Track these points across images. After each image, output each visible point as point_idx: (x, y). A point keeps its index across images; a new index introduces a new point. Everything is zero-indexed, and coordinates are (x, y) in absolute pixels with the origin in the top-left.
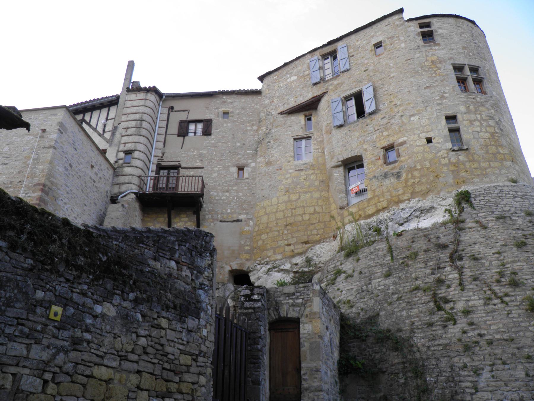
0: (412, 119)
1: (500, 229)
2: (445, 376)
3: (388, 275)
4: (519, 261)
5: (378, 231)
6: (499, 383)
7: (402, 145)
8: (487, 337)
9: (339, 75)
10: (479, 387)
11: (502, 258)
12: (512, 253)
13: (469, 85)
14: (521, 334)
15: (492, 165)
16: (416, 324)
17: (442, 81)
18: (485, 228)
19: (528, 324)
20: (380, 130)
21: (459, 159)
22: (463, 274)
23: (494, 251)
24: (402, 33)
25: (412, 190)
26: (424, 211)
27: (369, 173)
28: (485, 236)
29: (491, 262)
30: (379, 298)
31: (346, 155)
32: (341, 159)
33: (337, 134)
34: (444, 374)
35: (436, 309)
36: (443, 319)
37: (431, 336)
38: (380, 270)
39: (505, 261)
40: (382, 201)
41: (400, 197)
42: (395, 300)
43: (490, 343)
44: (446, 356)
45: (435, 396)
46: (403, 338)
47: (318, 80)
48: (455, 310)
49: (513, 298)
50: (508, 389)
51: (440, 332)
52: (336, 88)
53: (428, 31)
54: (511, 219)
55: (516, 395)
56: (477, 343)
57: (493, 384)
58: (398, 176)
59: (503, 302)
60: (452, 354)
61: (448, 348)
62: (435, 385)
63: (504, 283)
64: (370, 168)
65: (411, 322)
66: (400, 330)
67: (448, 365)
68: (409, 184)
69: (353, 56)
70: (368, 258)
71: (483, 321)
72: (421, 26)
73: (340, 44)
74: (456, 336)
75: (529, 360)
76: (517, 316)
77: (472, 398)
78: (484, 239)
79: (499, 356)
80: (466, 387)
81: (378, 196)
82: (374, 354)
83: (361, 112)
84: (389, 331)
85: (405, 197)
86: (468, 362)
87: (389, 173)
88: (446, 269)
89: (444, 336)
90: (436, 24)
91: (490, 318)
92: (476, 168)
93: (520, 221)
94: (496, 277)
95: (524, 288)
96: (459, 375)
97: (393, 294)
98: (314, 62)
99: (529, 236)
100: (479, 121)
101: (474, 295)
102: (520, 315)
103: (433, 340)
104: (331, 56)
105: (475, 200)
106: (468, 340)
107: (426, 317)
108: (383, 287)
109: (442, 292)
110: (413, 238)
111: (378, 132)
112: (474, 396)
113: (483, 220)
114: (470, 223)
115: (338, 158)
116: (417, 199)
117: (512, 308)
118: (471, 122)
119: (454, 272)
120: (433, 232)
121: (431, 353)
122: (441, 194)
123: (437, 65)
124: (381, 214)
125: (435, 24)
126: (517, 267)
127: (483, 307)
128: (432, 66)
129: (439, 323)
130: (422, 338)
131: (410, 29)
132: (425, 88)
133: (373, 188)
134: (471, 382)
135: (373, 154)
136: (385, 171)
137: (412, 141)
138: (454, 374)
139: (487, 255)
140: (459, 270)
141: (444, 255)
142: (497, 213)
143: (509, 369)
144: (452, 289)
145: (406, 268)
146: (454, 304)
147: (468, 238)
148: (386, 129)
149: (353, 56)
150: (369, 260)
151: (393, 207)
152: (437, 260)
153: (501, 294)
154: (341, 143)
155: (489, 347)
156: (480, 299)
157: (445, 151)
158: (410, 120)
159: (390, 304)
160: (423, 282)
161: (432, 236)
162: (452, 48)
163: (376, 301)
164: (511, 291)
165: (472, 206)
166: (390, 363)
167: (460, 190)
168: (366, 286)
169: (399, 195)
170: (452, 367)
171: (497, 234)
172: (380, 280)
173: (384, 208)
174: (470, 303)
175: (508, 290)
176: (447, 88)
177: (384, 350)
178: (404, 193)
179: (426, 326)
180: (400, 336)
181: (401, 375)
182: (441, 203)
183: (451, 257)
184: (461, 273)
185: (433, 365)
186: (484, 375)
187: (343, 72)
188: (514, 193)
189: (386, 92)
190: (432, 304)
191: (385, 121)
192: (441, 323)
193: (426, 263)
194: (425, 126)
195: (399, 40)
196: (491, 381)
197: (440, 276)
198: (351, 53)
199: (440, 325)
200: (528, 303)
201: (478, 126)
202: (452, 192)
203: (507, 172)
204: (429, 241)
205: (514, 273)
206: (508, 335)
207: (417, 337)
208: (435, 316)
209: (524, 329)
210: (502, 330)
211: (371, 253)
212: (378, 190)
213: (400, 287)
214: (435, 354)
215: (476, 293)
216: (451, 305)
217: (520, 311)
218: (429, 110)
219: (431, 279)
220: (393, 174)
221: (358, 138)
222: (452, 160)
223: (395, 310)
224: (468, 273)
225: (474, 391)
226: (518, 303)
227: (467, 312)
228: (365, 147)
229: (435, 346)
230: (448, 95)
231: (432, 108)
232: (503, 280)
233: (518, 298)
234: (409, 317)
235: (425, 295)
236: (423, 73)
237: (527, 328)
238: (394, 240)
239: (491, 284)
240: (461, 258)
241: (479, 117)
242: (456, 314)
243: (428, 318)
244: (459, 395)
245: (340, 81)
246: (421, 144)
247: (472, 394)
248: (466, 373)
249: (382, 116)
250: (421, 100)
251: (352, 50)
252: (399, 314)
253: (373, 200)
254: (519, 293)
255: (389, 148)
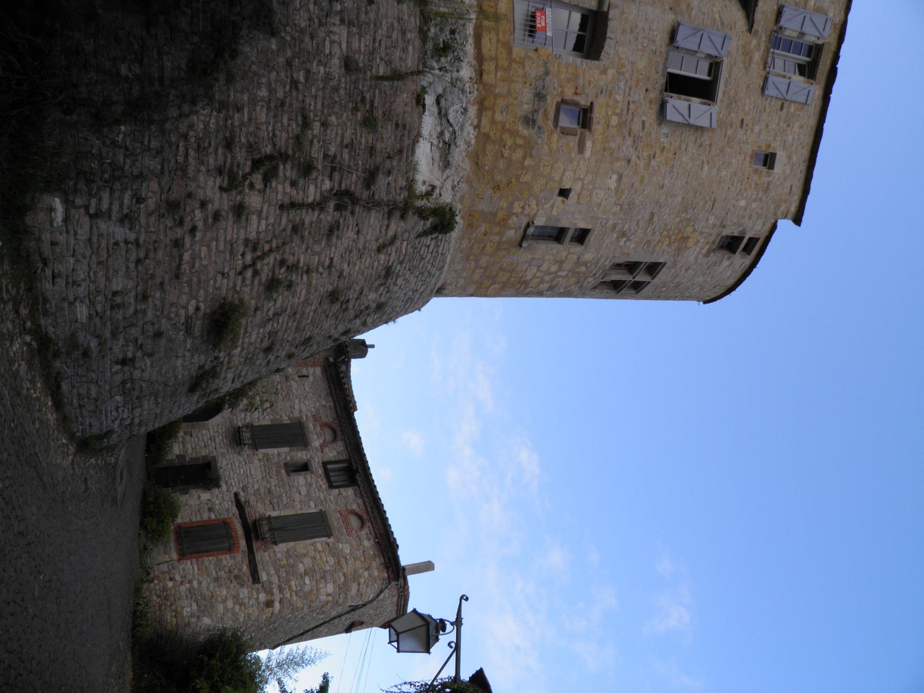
0: (615, 177)
1: (370, 271)
2: (125, 163)
3: (349, 64)
4: (308, 292)
5: (444, 50)
6: (104, 255)
7: (579, 145)
8: (188, 240)
9: (765, 68)
10: (99, 221)
11: (321, 270)
12: (323, 283)
13: (618, 274)
14: (187, 290)
15: (479, 271)
16: (236, 116)
17: (648, 242)
18: (379, 250)
19: (200, 299)
20: (625, 112)
21: (510, 228)
22: (310, 210)
23: (335, 260)
24: (762, 208)
25: (493, 138)
26: (446, 148)
27: (559, 65)
28: (365, 248)
29: (319, 254)
30: (307, 39)
31: (614, 27)
32: (611, 14)
33: (662, 21)
34: (128, 161)
35: (258, 157)
36: (235, 169)
37: (206, 144)
38: (362, 49)
39: (314, 274)
40: (496, 75)
41: (489, 113)
42: (295, 75)
43: (177, 243)
44: (162, 168)
45: (86, 139)
46: (212, 87)
47: (783, 22)
48: (247, 190)
49: (248, 282)
50: (94, 267)
51: (211, 161)
52: (747, 54)
53: (738, 247)
54: (381, 285)
55: (82, 276)
56: (181, 223)
57: (104, 244)
58: (529, 121)
59: (245, 267)
60: (165, 180)
61: (179, 173)
62: (108, 142)
63: (277, 271)
64: (567, 68)
65: (243, 105)
66: (230, 79)
67: (145, 171)
68: (506, 136)
69: (782, 108)
70: (396, 25)
71: (217, 236)
72: (752, 241)
73: (817, 90)
74: (199, 190)
75: (140, 297)
76: (217, 286)
77: (80, 207)
78: (361, 247)
79: (152, 255)
80: (100, 199)
81: (508, 69)
82: (189, 12)
83: (679, 85)
84: (234, 54)
85: (485, 122)
86: (146, 206)
87: (542, 104)
88: (327, 182)
89: (203, 168)
90: (740, 261)
91: (222, 248)
92: (484, 248)
93: (372, 296)
94: (291, 260)
95: (262, 297)
96: (124, 189)
97: (308, 71)
98: (821, 27)
99: (344, 306)
100: (556, 272)
101: (267, 225)
102: (219, 289)
103: (199, 146)
104: (808, 62)
105: (432, 239)
106: (188, 210)
107: (246, 137)
108: (327, 51)
109: (287, 171)
110: (405, 126)
111: (625, 108)
112: (82, 211)
113: (394, 249)
114: (395, 226)
115: (617, 7)
116: (473, 141)
117: (232, 280)
118: (561, 262)
119: (318, 195)
120: (403, 165)
121: (173, 140)
122: (464, 186)
123: (677, 244)
124: (474, 62)
125: (741, 261)
126: (299, 291)
127: (242, 236)
128: (680, 235)
129: (229, 161)
130: (206, 125)
131: (760, 222)
132: (652, 215)
133: (528, 63)
134: (110, 210)
135: (589, 83)
136: (549, 98)
137: (578, 165)
138: (126, 180)
139: (333, 248)
140: (319, 204)
141: (353, 181)
142: (399, 268)
143: (128, 268)
144: (288, 189)
145: (351, 105)
146: (259, 191)
147: (372, 223)
148: (621, 125)
149: (782, 108)
150: (392, 25)
151: (476, 93)
152: (349, 167)
153: (259, 266)
154: (640, 25)
155: (171, 240)
156: (258, 232)
157: (533, 213)
158: (614, 172)
159: (289, 64)
160: (314, 136)
161: (395, 163)
162: (690, 271)
163: (302, 31)
164: (260, 280)
165: (425, 233)
166: (166, 49)
167: (458, 219)
168: (341, 12)
169: (494, 112)
170: (141, 177)
171: (362, 267)
172: (344, 46)
173: (481, 74)
174: (254, 218)
175: (264, 276)
176: (633, 246)
177: (196, 39)
178: (493, 122)
179: (228, 134)
180: (217, 80)
181: (137, 69)
182: (450, 181)
183: (347, 193)
184: (312, 206)
185: (149, 141)
186: (121, 229)
187: (766, 79)
188: (421, 291)
189: (684, 146)
190: (268, 150)
191: (636, 127)
192: (228, 165)
193: (350, 146)
194: (591, 196)
195: (755, 200)
196: (108, 240)
197: (318, 170)
198: (789, 107)
199: (225, 162)
200: (236, 302)
201: (549, 269)
202: (461, 203)
203: (459, 285)
204: (389, 157)
205: (290, 286)
206: (188, 271)
207: (210, 115)
208: (244, 154)
209: (194, 293)
210: (197, 264)
211: (404, 33)
212: (520, 72)
213: (318, 89)
214: (170, 147)
215: (270, 227)
216: (259, 185)
217: (224, 290)
218: (615, 208)
219: (316, 152)
220: (536, 111)
221: (633, 63)
222: (515, 218)
223: (274, 74)
224: (309, 217)
225: (92, 211)
226: (238, 289)
227: (239, 210)
228: (611, 72)
229: (187, 150)
230: (622, 243)
231: (614, 214)
232: (283, 270)
233: (247, 289)
234: (254, 101)
235: (288, 138)
236: (678, 219)
237: (196, 298)
238: (413, 87)
239: (281, 252)
240: (338, 208)
241: (563, 274)
242: (240, 192)
243: (243, 140)
244: (86, 185)
245: (753, 66)
246: (564, 178)
247: (87, 208)
248: (126, 201)
249: (647, 125)
250: (637, 202)
251: (792, 109)
252: (264, 80)
253: (505, 55)
254: (255, 290)
255: (585, 117)
